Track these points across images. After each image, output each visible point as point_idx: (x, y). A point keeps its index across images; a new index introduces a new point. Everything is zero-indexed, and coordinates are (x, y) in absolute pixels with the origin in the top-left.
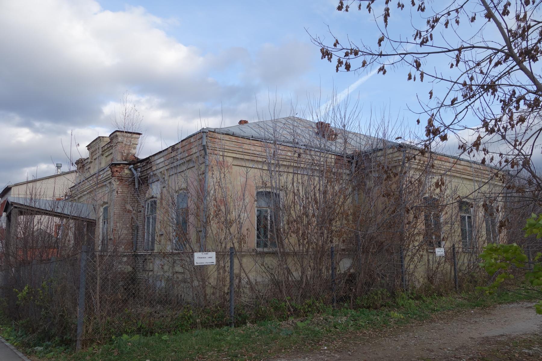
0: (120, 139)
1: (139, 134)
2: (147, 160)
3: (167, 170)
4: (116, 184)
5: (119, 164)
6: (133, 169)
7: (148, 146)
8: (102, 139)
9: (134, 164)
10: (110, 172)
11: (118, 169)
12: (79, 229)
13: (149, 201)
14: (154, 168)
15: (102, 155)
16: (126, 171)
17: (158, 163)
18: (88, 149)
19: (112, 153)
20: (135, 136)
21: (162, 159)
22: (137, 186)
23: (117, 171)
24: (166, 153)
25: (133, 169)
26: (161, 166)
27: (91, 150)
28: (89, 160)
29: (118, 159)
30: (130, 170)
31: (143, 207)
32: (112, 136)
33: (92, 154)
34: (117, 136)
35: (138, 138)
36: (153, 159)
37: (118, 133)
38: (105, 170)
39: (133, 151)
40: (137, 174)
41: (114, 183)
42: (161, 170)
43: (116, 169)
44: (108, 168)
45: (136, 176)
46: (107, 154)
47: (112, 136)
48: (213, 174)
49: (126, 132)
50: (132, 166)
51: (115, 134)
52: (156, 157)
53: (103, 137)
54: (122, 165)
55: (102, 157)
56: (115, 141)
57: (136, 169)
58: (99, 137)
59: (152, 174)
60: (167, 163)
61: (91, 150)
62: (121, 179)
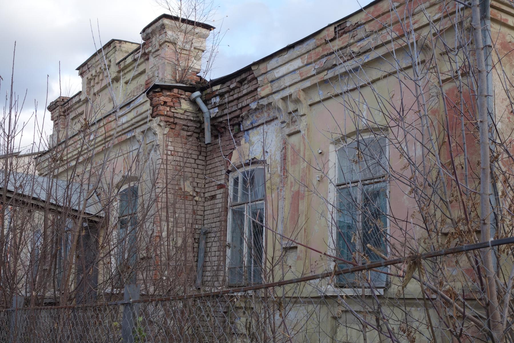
0: (170, 34)
1: (209, 27)
2: (245, 75)
3: (305, 90)
4: (160, 131)
5: (170, 88)
6: (199, 101)
7: (221, 57)
8: (118, 45)
9: (202, 90)
10: (148, 105)
11: (168, 100)
12: (56, 239)
13: (239, 174)
14: (262, 92)
15: (116, 80)
16: (185, 105)
17: (277, 75)
18: (81, 74)
19: (144, 72)
20: (199, 30)
21: (298, 63)
22: (208, 138)
23: (165, 103)
24: (312, 43)
25: (199, 101)
26: (287, 81)
27: (88, 75)
28: (83, 97)
29: (166, 77)
30: (193, 102)
31: (221, 186)
32: (149, 30)
33: (88, 83)
34: (163, 27)
35: (205, 37)
36: (257, 71)
37: (166, 21)
38: (132, 105)
39: (196, 65)
40: (209, 113)
41: (158, 130)
42: (286, 93)
43: (163, 99)
44: (144, 98)
45: (207, 115)
46: (130, 76)
47: (149, 30)
48: (158, 325)
49: (183, 21)
50: (197, 93)
51: (160, 22)
52: (273, 63)
53: (120, 41)
54: (176, 91)
55: (115, 85)
56: (155, 41)
57: (206, 102)
58: (113, 41)
59: (253, 106)
60: (311, 70)
61: (88, 75)
62: (171, 123)
